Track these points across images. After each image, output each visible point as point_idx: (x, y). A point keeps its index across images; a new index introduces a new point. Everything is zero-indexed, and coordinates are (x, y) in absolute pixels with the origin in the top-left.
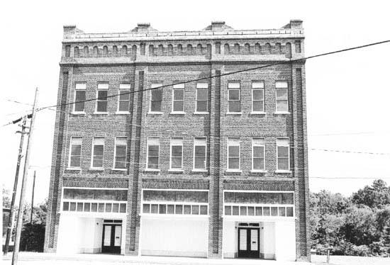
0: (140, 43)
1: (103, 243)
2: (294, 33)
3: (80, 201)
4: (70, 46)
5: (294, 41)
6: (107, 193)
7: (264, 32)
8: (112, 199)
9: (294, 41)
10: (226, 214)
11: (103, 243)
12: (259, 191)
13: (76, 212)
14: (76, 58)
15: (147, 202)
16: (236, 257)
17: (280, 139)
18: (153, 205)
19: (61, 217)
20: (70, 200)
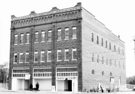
0: (31, 19)
1: (55, 87)
2: (78, 8)
3: (39, 73)
4: (80, 11)
5: (78, 11)
6: (24, 70)
7: (69, 9)
8: (25, 73)
9: (78, 11)
10: (34, 76)
11: (55, 87)
12: (67, 68)
13: (16, 77)
14: (16, 26)
15: (35, 73)
16: (64, 91)
17: (66, 49)
18: (36, 74)
19: (12, 79)
20: (14, 73)
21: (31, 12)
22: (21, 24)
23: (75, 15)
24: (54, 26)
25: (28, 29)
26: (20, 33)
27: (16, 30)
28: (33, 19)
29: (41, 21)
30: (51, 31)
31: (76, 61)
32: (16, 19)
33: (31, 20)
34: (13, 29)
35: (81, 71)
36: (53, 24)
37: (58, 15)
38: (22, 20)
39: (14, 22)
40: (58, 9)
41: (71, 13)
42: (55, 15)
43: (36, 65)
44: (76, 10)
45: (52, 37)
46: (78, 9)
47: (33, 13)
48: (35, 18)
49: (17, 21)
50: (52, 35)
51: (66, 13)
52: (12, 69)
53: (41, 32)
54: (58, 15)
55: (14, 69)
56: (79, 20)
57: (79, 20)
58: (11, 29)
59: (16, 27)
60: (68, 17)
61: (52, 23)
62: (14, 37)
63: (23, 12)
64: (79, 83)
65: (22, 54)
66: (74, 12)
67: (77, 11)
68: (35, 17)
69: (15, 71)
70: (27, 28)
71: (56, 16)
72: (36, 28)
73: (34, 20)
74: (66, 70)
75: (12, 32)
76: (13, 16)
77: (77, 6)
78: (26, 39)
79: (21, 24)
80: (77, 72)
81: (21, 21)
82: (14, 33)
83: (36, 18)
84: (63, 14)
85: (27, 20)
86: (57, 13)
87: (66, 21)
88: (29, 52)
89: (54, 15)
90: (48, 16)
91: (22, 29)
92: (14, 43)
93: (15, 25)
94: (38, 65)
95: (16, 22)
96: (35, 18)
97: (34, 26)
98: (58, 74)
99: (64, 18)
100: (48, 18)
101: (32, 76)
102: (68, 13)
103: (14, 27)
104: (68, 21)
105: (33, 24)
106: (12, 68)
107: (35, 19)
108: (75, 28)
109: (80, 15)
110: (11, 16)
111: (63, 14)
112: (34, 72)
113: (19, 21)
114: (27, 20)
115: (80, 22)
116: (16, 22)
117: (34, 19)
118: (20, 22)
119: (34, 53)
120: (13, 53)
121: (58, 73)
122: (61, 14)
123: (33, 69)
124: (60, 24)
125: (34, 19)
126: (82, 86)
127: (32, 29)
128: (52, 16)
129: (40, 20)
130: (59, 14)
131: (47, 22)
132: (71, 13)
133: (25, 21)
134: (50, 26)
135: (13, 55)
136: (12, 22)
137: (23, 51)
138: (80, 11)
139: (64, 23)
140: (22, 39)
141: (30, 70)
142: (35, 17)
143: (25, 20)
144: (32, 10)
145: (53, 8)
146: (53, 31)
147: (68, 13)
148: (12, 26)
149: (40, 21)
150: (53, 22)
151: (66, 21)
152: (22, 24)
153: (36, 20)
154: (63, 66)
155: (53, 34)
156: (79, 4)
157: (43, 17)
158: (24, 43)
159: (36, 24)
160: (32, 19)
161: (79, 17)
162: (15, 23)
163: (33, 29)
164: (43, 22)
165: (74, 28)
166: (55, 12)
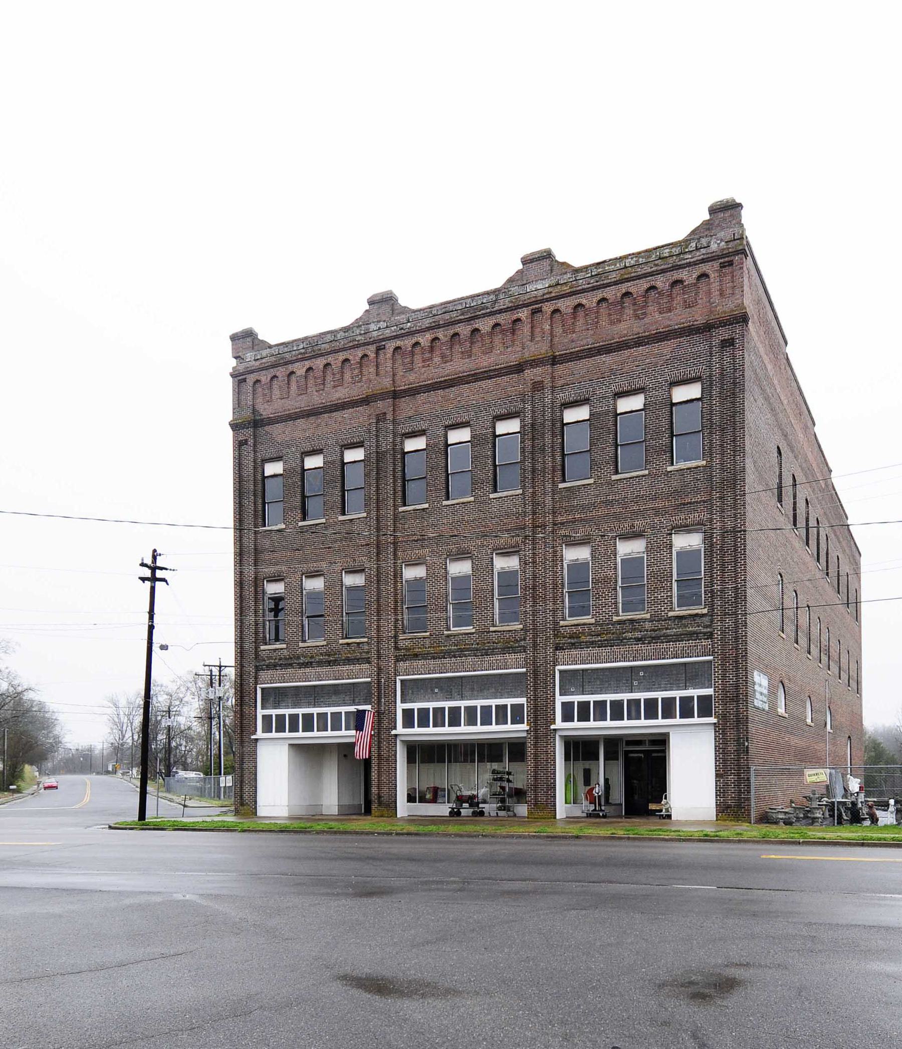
0: (373, 348)
4: (731, 263)
5: (716, 264)
9: (716, 264)
14: (278, 393)
21: (371, 302)
22: (303, 390)
23: (690, 296)
24: (537, 386)
25: (356, 420)
26: (293, 453)
27: (267, 428)
28: (245, 380)
29: (443, 356)
30: (513, 426)
31: (703, 615)
32: (265, 353)
33: (372, 355)
34: (250, 429)
35: (737, 687)
36: (530, 374)
37: (566, 305)
38: (307, 364)
39: (251, 379)
40: (564, 264)
41: (661, 282)
42: (539, 311)
43: (416, 656)
44: (703, 261)
45: (523, 461)
46: (720, 248)
47: (384, 302)
48: (399, 343)
49: (272, 372)
50: (523, 450)
51: (624, 288)
52: (256, 683)
53: (441, 432)
54: (563, 309)
55: (270, 680)
56: (721, 330)
57: (723, 333)
58: (234, 426)
59: (266, 410)
60: (637, 317)
61: (519, 368)
62: (259, 477)
63: (314, 306)
64: (725, 760)
65: (460, 568)
66: (683, 274)
67: (705, 268)
68: (396, 337)
69: (275, 697)
70: (347, 413)
71: (251, 384)
72: (407, 406)
73: (394, 360)
74: (450, 688)
75: (239, 445)
76: (245, 340)
77: (706, 228)
78: (343, 490)
79: (303, 390)
80: (522, 700)
81: (300, 369)
82: (255, 452)
83: (407, 343)
84: (604, 300)
85: (341, 356)
86: (555, 292)
87: (623, 345)
88: (362, 571)
89: (534, 312)
90: (491, 321)
91: (312, 419)
92: (261, 517)
93: (259, 400)
94: (432, 650)
95: (265, 377)
96: (399, 343)
97: (396, 395)
98: (267, 719)
99: (612, 323)
100: (491, 334)
101: (553, 721)
102: (638, 288)
103: (254, 411)
104: (640, 342)
105: (386, 383)
106: (256, 678)
107: (398, 348)
108: (693, 391)
109: (729, 291)
110: (234, 338)
111: (600, 296)
112: (403, 701)
113: (290, 367)
114: (341, 356)
115: (729, 343)
116: (265, 377)
117: (391, 346)
118: (293, 373)
119: (557, 558)
120: (257, 583)
121: (267, 712)
122: (584, 302)
123: (558, 668)
124: (581, 367)
125: (548, 308)
126: (749, 786)
127: (381, 418)
128: (518, 320)
129: (432, 349)
130: (571, 302)
131: (485, 362)
132: (661, 282)
133: (327, 365)
134: (512, 385)
135: (258, 591)
136: (239, 378)
137: (324, 565)
138: (731, 263)
139: (607, 360)
140: (355, 477)
141: (374, 691)
142: (396, 337)
143: (330, 359)
144: (379, 288)
145: (526, 261)
146: (528, 420)
147: (638, 288)
148: (238, 404)
149: (437, 359)
150: (527, 355)
151: (623, 345)
152: (312, 389)
153: (403, 355)
154: (605, 651)
155: (528, 443)
156: (726, 211)
157: (461, 322)
158: (327, 509)
159: (565, 343)
160: (378, 349)
161: (725, 307)
162: (258, 381)
163: (389, 416)
164: (459, 365)
165: (681, 394)
166: (539, 287)
